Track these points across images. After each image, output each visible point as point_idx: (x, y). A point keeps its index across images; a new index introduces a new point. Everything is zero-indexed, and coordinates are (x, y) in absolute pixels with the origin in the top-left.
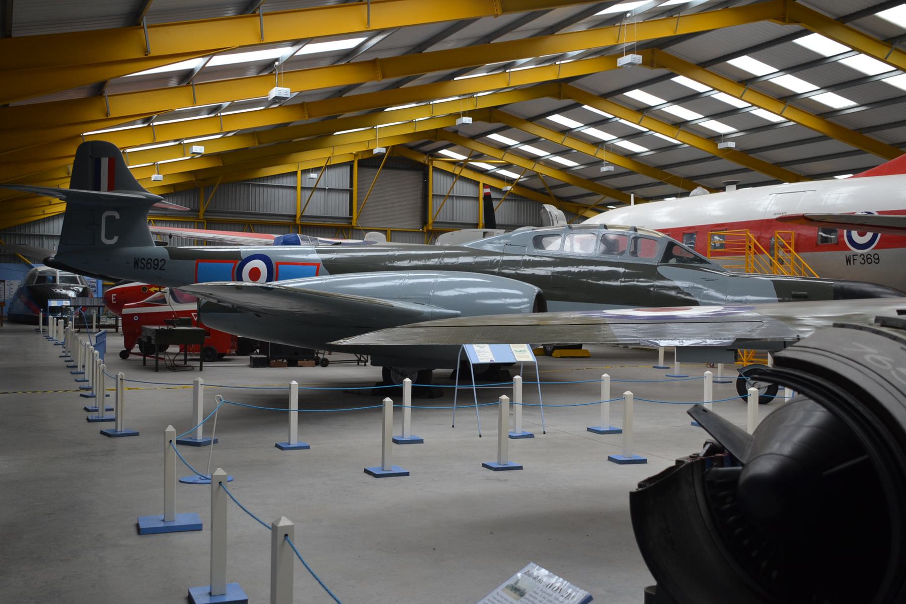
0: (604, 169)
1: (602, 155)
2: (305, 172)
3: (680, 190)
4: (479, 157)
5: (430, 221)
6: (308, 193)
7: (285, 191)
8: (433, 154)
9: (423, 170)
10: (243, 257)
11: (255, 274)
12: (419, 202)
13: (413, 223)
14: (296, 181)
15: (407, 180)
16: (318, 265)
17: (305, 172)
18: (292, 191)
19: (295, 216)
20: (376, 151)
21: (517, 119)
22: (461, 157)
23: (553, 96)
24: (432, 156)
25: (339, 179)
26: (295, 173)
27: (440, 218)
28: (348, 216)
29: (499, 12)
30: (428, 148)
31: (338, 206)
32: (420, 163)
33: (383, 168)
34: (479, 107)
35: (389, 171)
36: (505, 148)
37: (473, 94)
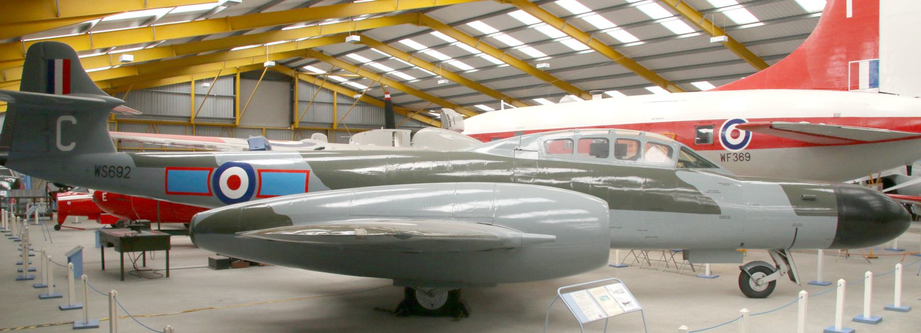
0: (440, 82)
1: (384, 81)
2: (202, 81)
3: (492, 99)
4: (334, 72)
6: (201, 99)
7: (181, 97)
8: (298, 69)
9: (291, 81)
11: (234, 182)
13: (284, 123)
15: (281, 88)
23: (413, 23)
24: (298, 70)
25: (225, 87)
26: (190, 83)
27: (305, 119)
28: (232, 117)
31: (224, 110)
32: (288, 76)
36: (359, 65)
37: (352, 17)
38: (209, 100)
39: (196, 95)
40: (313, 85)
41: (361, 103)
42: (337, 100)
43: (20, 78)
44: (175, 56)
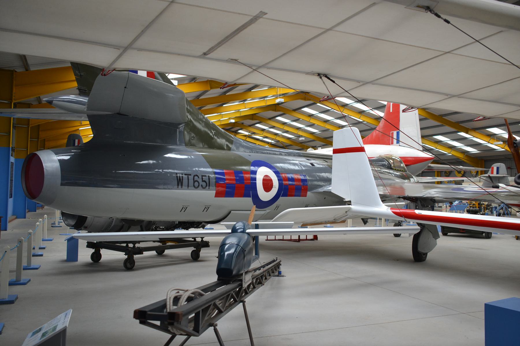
4: (254, 133)
21: (290, 111)
22: (247, 133)
24: (236, 133)
30: (234, 130)
36: (311, 116)
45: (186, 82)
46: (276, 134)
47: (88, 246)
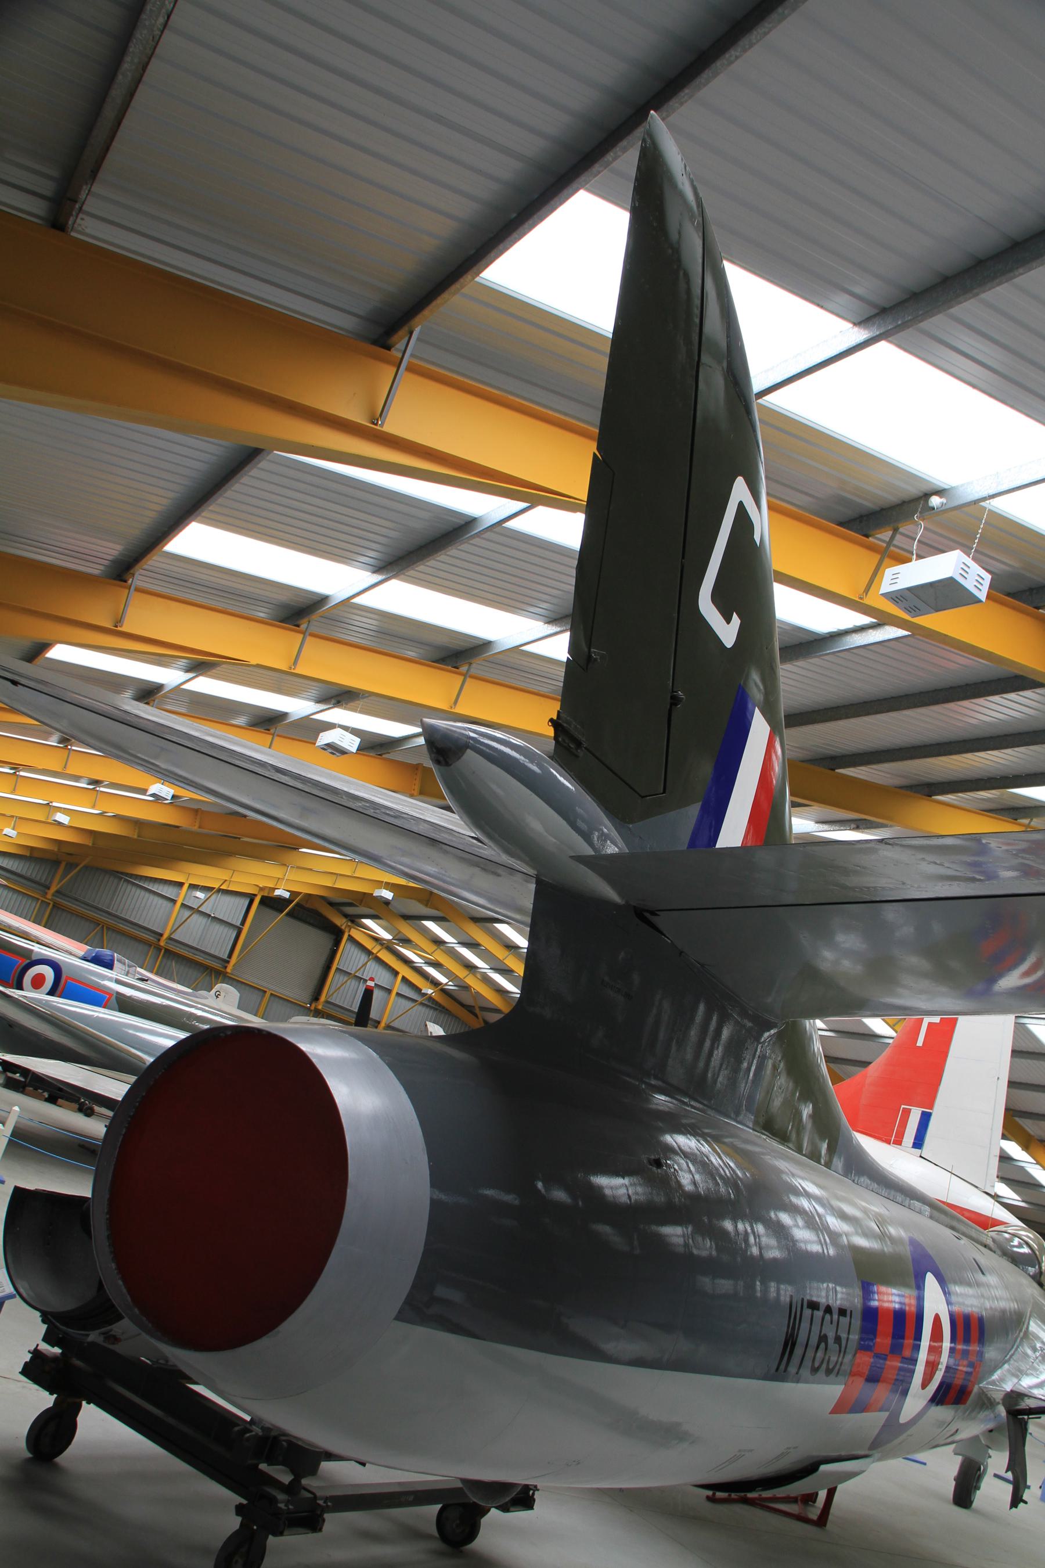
2: (193, 887)
4: (406, 942)
5: (323, 998)
6: (187, 913)
7: (161, 901)
8: (354, 920)
9: (337, 934)
10: (34, 958)
12: (318, 972)
14: (178, 895)
16: (111, 995)
17: (193, 887)
18: (170, 904)
19: (161, 935)
20: (277, 893)
22: (386, 936)
24: (353, 922)
25: (231, 909)
26: (181, 884)
27: (336, 999)
28: (225, 957)
29: (416, 793)
30: (350, 910)
32: (336, 926)
33: (288, 914)
34: (336, 886)
35: (288, 919)
36: (438, 942)
38: (195, 917)
39: (183, 905)
40: (369, 952)
41: (431, 1004)
42: (398, 986)
43: (356, 1010)
44: (195, 828)
45: (241, 721)
46: (470, 967)
47: (28, 1371)
